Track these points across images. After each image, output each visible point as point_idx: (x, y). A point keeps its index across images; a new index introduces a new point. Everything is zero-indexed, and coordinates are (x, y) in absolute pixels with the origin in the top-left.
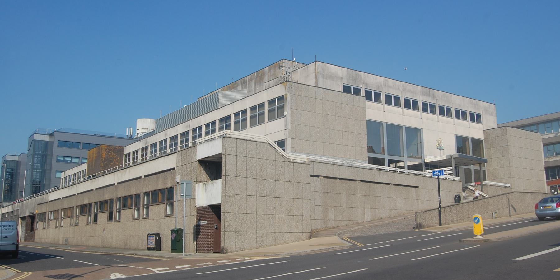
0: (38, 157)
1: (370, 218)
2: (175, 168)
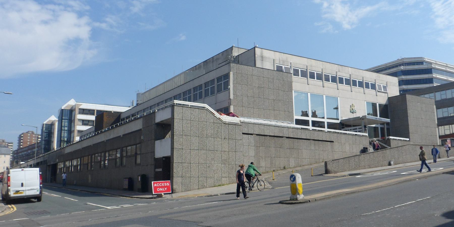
0: (65, 122)
2: (141, 129)
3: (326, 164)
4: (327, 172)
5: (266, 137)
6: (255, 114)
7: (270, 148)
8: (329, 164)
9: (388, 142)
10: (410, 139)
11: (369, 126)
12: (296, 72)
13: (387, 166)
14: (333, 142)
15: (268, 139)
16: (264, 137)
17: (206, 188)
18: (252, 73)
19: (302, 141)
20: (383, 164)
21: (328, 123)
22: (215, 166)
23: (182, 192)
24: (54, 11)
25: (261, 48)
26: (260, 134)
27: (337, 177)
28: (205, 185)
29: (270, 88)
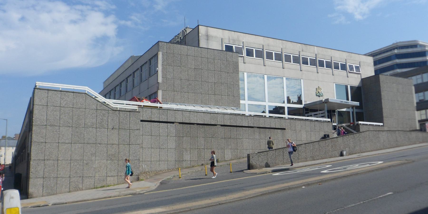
1: (230, 157)
3: (248, 156)
4: (250, 167)
5: (191, 125)
6: (189, 100)
7: (198, 139)
8: (253, 157)
9: (357, 128)
10: (383, 124)
11: (338, 110)
12: (249, 53)
13: (338, 157)
14: (285, 129)
15: (194, 127)
16: (189, 125)
17: (80, 190)
18: (187, 53)
19: (243, 129)
20: (332, 155)
21: (288, 107)
22: (96, 163)
23: (43, 196)
24: (82, 11)
25: (207, 26)
26: (185, 122)
27: (256, 174)
28: (81, 186)
29: (210, 69)
